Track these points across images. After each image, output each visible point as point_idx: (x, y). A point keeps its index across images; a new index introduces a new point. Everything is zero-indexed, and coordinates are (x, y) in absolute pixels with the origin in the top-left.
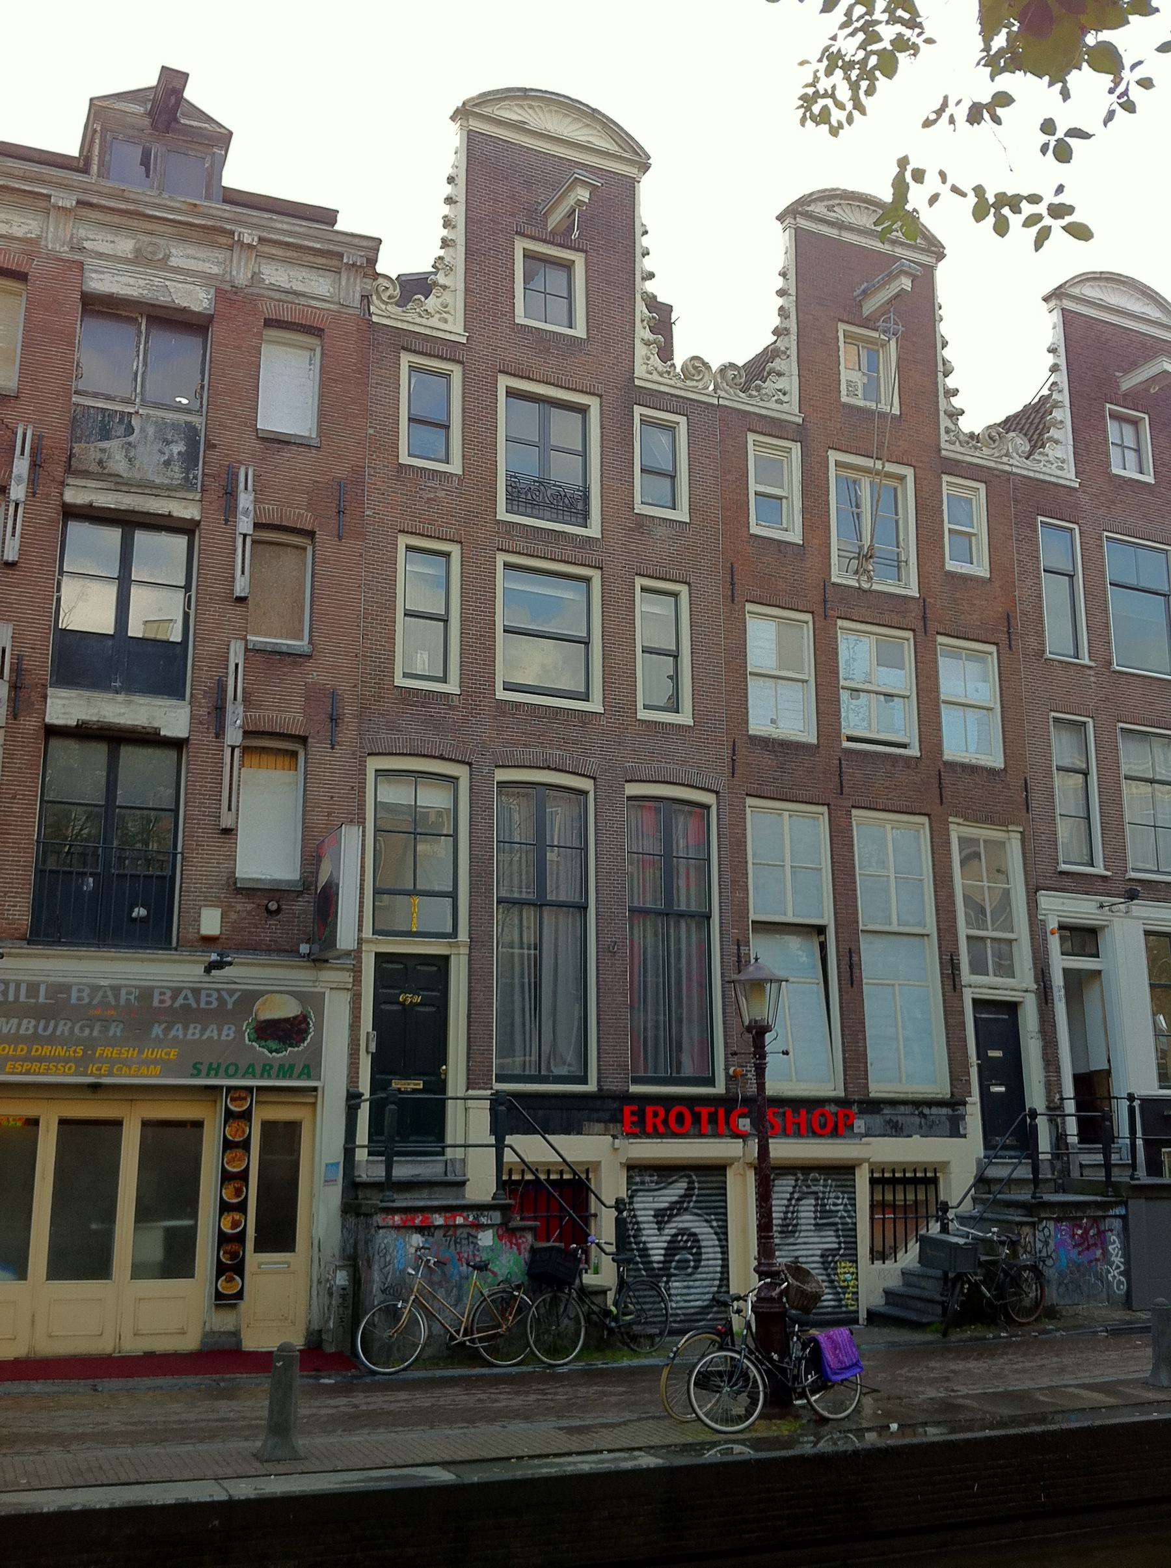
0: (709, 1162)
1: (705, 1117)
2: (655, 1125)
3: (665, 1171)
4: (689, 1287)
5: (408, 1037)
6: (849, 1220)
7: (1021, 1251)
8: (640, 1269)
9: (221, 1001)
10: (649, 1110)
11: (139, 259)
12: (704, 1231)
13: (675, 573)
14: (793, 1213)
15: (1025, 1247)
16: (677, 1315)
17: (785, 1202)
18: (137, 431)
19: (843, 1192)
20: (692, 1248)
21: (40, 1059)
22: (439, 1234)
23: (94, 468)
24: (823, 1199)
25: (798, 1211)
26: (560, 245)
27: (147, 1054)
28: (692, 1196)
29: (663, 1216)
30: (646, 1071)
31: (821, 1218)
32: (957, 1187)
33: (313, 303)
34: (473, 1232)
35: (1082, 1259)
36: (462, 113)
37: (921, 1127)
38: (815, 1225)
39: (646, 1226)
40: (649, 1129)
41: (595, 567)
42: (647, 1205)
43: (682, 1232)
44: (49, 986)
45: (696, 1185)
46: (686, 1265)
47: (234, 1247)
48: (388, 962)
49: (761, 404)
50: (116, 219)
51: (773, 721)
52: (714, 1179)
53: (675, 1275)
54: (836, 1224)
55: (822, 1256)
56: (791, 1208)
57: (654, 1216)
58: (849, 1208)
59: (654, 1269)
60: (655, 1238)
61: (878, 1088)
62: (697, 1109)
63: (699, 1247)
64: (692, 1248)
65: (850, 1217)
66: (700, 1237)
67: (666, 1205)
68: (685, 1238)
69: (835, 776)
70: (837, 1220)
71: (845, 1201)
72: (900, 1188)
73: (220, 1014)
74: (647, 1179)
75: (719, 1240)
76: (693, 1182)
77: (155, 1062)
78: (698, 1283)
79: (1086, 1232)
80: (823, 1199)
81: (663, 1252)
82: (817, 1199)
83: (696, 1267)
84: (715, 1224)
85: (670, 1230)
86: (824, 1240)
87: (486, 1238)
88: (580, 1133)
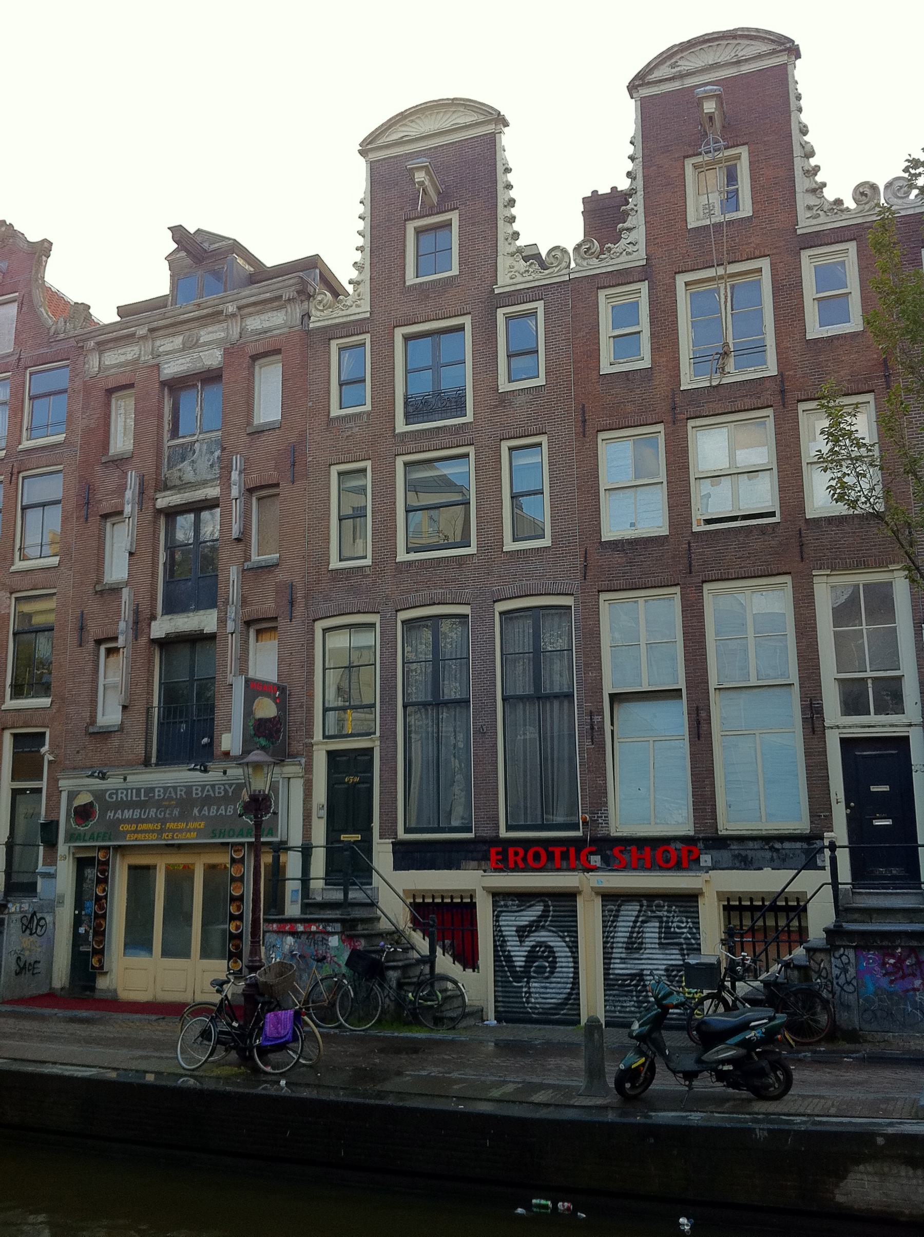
0: (534, 890)
1: (557, 855)
2: (516, 862)
3: (525, 897)
4: (546, 988)
5: (349, 804)
6: (693, 941)
7: (814, 976)
8: (506, 971)
9: (226, 790)
10: (511, 851)
11: (187, 347)
12: (558, 945)
13: (533, 429)
14: (638, 933)
15: (819, 973)
16: (536, 1008)
17: (631, 924)
18: (197, 452)
19: (687, 917)
20: (548, 957)
21: (142, 832)
22: (304, 937)
23: (178, 482)
24: (667, 922)
25: (643, 932)
26: (438, 213)
27: (190, 825)
28: (548, 916)
29: (524, 932)
30: (526, 820)
31: (665, 938)
32: (820, 917)
33: (275, 332)
34: (326, 937)
35: (895, 987)
36: (632, 88)
37: (772, 860)
38: (659, 944)
39: (509, 938)
40: (512, 865)
41: (468, 445)
42: (510, 923)
43: (540, 944)
44: (146, 789)
45: (551, 908)
46: (543, 970)
47: (237, 942)
48: (362, 755)
49: (614, 262)
50: (171, 330)
51: (632, 525)
52: (567, 904)
53: (534, 978)
54: (681, 944)
55: (666, 970)
56: (637, 929)
57: (516, 931)
58: (694, 931)
59: (516, 972)
60: (517, 948)
61: (728, 825)
62: (550, 849)
63: (555, 957)
64: (548, 957)
65: (694, 939)
66: (555, 949)
67: (527, 923)
68: (542, 949)
69: (691, 558)
70: (682, 941)
71: (690, 925)
72: (747, 914)
73: (226, 799)
74: (510, 903)
75: (572, 952)
76: (549, 906)
77: (195, 830)
78: (553, 985)
79: (900, 960)
80: (667, 922)
81: (524, 959)
82: (661, 922)
83: (552, 972)
84: (567, 939)
85: (529, 942)
86: (669, 957)
87: (334, 941)
88: (458, 868)
